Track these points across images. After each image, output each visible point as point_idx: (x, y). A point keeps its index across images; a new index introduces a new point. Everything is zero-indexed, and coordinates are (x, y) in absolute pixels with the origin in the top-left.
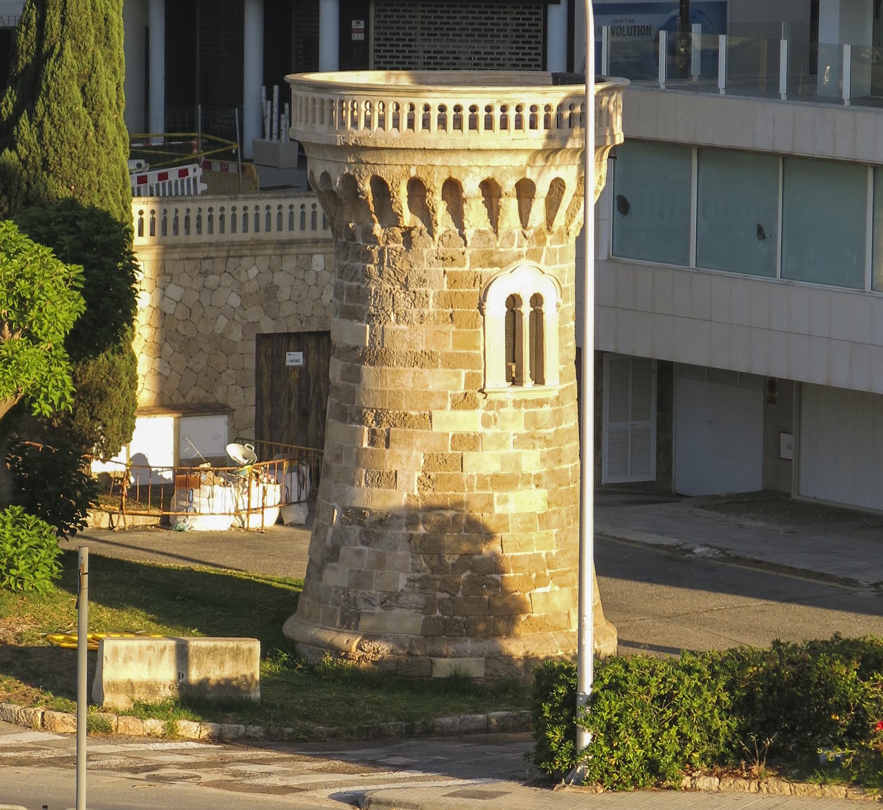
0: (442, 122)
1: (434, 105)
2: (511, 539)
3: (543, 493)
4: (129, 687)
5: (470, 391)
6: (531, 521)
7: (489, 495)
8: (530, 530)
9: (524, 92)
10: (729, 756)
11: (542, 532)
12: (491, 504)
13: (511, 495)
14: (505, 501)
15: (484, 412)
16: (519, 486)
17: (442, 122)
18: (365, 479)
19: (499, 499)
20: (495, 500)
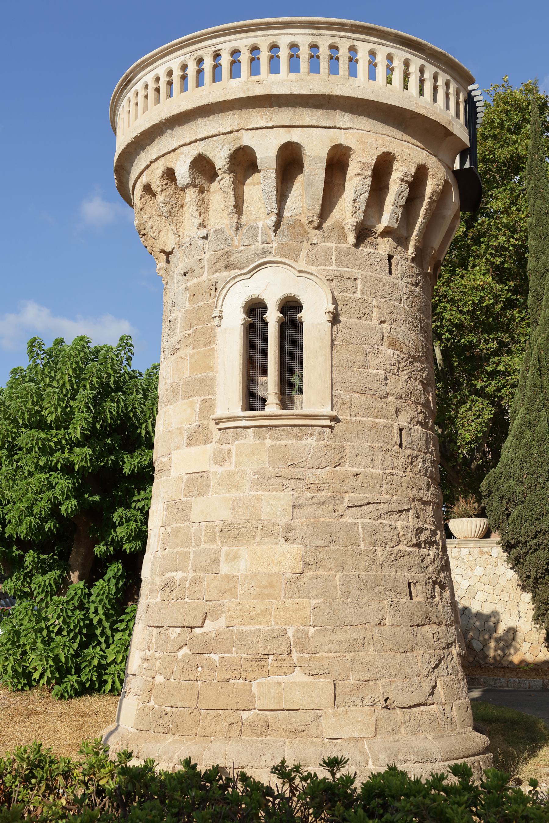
0: (274, 60)
1: (264, 44)
2: (238, 608)
3: (296, 548)
4: (313, 49)
5: (204, 422)
6: (271, 585)
7: (216, 550)
8: (268, 596)
9: (381, 44)
10: (25, 761)
11: (288, 601)
12: (216, 562)
13: (244, 550)
14: (236, 558)
15: (217, 445)
16: (257, 539)
17: (274, 60)
18: (407, 360)
19: (227, 555)
20: (223, 556)
